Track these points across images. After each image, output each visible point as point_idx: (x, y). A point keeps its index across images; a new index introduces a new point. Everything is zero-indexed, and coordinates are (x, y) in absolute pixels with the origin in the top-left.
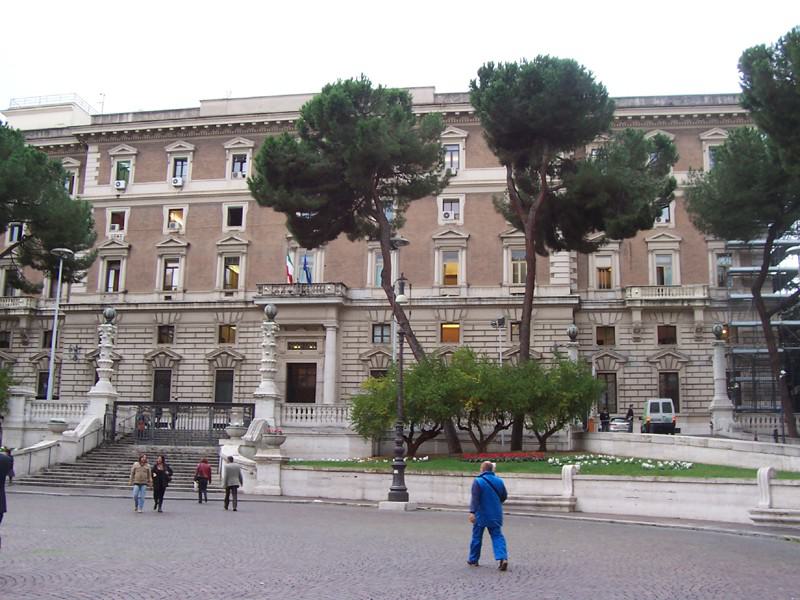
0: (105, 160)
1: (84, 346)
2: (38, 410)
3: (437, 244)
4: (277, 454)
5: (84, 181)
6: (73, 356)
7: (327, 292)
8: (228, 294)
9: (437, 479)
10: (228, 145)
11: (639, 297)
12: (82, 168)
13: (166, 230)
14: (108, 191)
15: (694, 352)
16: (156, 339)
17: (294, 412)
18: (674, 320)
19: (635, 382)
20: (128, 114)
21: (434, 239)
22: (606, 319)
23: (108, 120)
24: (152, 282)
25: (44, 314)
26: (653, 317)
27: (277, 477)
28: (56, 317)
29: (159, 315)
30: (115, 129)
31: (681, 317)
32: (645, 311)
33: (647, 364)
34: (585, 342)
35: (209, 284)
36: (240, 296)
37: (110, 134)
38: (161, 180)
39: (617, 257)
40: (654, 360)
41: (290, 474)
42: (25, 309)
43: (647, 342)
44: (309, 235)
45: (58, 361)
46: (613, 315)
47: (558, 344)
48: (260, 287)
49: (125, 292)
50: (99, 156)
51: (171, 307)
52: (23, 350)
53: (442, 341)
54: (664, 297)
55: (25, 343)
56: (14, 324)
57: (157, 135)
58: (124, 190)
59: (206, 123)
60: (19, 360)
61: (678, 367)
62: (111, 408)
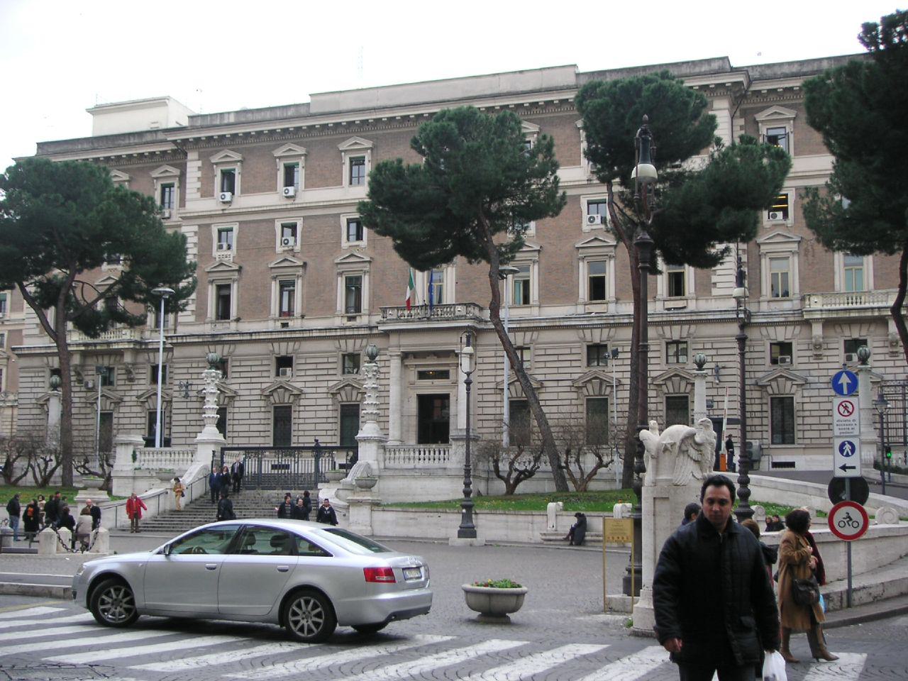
0: (207, 168)
1: (195, 382)
2: (147, 457)
3: (581, 254)
4: (367, 497)
5: (185, 192)
6: (183, 394)
7: (457, 313)
8: (350, 319)
9: (511, 518)
10: (278, 153)
11: (819, 307)
12: (182, 177)
13: (279, 249)
14: (210, 205)
15: (889, 370)
16: (340, 371)
17: (417, 453)
18: (864, 332)
19: (816, 407)
20: (229, 113)
21: (578, 248)
22: (781, 334)
23: (208, 122)
24: (267, 307)
25: (150, 347)
26: (838, 330)
27: (368, 519)
28: (161, 350)
29: (276, 345)
30: (215, 133)
31: (872, 329)
32: (828, 323)
33: (573, 389)
34: (757, 362)
35: (329, 309)
36: (363, 320)
37: (210, 139)
38: (271, 190)
39: (796, 259)
40: (764, 382)
41: (379, 516)
42: (129, 342)
43: (830, 359)
44: (422, 255)
45: (168, 398)
46: (790, 328)
47: (720, 365)
48: (384, 310)
49: (238, 320)
50: (199, 163)
51: (288, 336)
52: (129, 388)
53: (344, 373)
54: (850, 306)
55: (131, 380)
56: (118, 359)
57: (314, 133)
58: (229, 203)
59: (317, 122)
60: (126, 399)
61: (793, 391)
62: (218, 454)
